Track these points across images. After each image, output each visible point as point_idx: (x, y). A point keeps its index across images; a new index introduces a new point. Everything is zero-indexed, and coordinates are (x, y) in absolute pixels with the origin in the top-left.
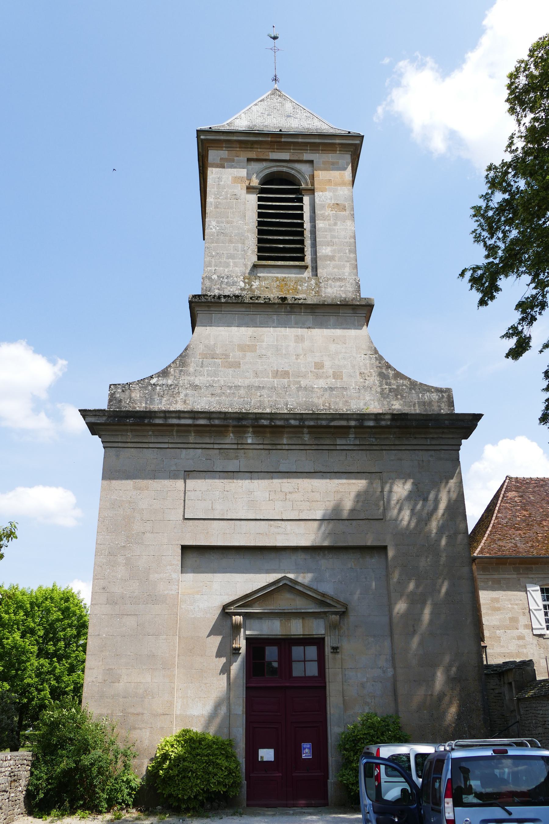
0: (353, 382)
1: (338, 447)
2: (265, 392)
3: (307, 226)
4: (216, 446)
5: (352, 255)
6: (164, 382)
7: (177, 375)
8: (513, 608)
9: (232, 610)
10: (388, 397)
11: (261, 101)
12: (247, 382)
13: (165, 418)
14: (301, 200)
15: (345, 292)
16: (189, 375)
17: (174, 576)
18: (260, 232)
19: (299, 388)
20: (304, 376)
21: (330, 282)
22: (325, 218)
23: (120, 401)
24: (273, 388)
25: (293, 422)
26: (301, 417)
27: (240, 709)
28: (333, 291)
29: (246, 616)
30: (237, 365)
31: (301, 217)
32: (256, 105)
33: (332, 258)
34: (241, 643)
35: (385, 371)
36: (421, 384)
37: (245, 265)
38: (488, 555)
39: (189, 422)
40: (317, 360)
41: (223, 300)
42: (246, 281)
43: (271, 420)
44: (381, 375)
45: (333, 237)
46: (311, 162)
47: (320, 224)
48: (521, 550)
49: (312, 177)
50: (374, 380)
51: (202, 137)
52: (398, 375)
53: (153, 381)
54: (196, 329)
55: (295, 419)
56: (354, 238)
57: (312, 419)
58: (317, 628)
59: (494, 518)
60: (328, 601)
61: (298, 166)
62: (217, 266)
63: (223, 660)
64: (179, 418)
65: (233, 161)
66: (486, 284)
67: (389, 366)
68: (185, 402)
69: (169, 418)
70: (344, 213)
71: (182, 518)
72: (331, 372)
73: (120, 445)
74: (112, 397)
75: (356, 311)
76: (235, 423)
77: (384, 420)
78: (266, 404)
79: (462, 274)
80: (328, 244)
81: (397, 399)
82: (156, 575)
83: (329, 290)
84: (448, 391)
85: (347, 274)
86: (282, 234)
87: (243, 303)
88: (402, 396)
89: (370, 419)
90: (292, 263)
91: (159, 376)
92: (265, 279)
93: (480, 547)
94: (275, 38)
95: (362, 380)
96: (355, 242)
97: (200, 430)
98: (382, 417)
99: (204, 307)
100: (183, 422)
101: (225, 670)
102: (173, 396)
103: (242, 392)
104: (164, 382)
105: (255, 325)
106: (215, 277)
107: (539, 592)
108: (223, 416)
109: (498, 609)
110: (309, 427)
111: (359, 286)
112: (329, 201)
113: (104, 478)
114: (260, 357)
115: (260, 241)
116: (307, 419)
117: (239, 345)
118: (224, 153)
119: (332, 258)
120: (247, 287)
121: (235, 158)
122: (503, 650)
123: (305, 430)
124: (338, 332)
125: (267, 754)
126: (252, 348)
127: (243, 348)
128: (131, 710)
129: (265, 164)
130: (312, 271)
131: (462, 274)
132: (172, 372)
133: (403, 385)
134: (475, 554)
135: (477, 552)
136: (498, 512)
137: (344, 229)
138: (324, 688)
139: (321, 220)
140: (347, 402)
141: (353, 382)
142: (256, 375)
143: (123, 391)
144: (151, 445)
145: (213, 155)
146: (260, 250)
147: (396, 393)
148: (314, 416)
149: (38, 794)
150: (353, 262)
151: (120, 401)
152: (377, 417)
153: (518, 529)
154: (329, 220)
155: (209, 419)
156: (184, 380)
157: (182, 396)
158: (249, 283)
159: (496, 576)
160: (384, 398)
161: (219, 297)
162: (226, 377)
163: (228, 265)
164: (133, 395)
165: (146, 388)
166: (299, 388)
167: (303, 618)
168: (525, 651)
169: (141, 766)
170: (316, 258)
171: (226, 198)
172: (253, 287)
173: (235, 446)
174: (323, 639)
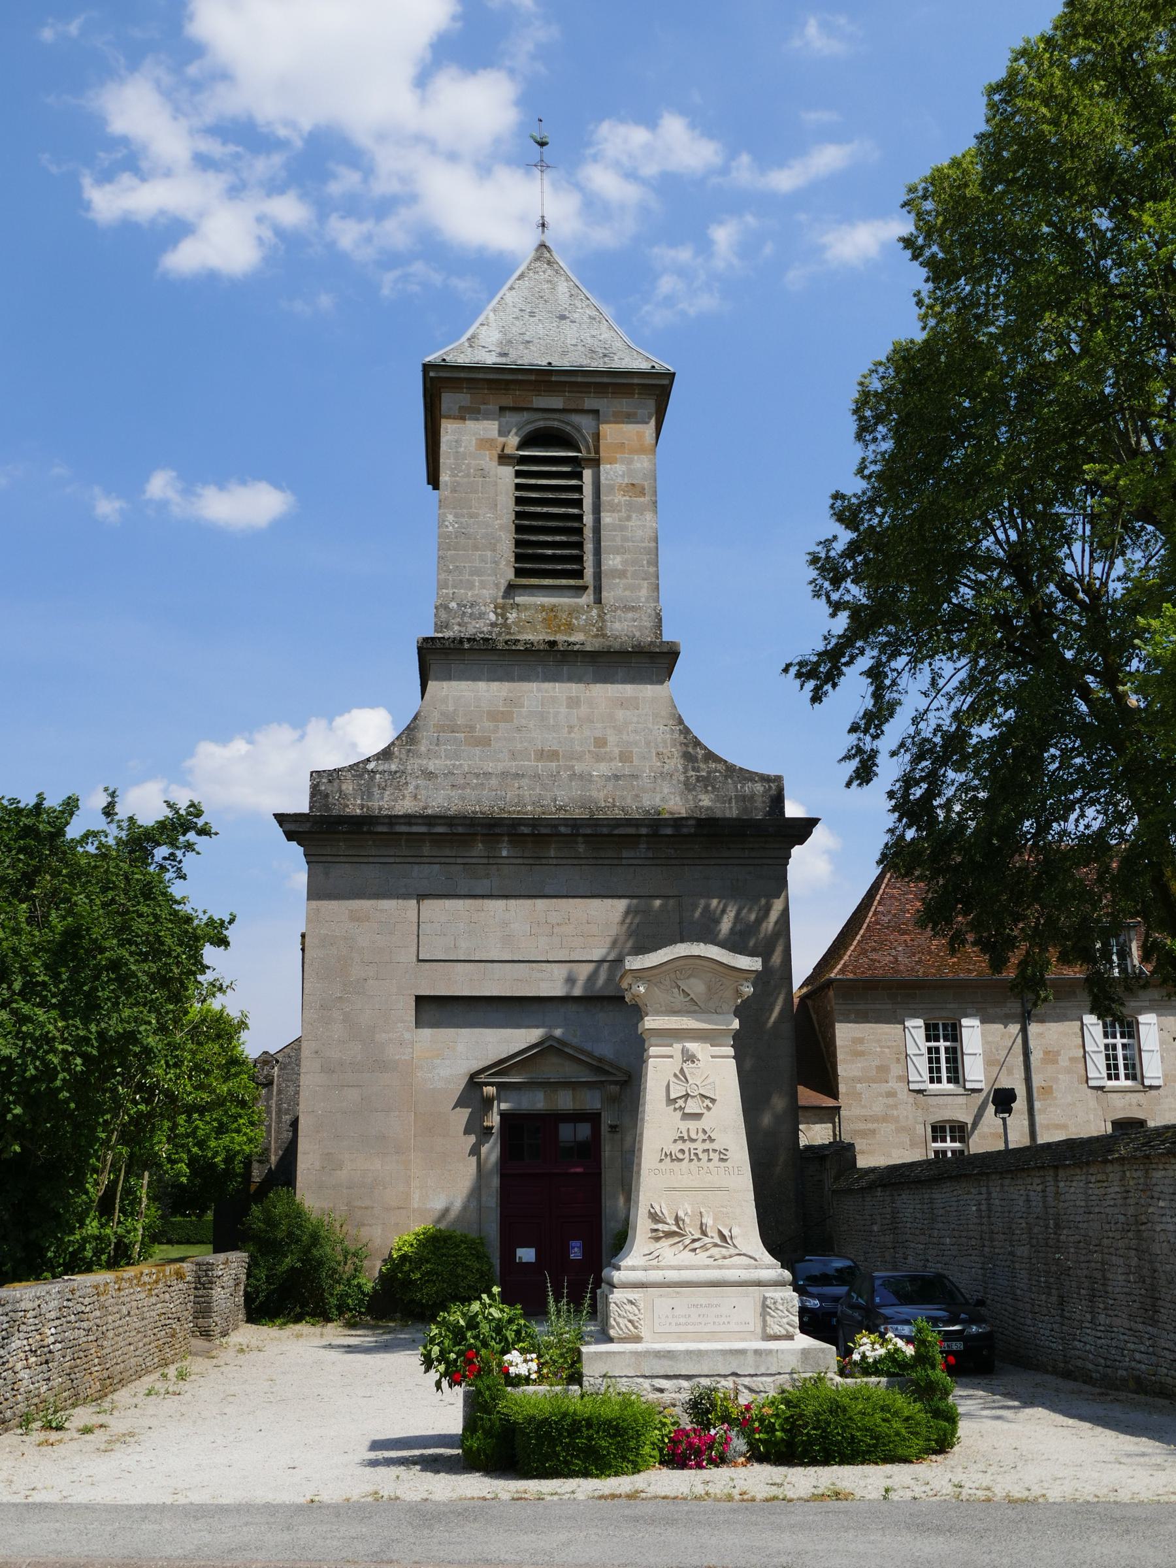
0: (647, 767)
1: (624, 862)
2: (525, 782)
3: (588, 519)
4: (459, 861)
5: (652, 569)
6: (386, 767)
7: (403, 756)
8: (883, 1052)
9: (482, 1078)
10: (694, 789)
11: (518, 279)
12: (500, 767)
13: (391, 824)
14: (579, 476)
15: (640, 628)
16: (420, 756)
17: (407, 1036)
18: (519, 529)
19: (573, 776)
20: (580, 759)
21: (619, 612)
22: (614, 508)
23: (327, 796)
24: (537, 776)
25: (563, 830)
26: (574, 823)
27: (492, 1200)
28: (624, 628)
29: (500, 1086)
30: (485, 742)
31: (579, 503)
32: (511, 288)
33: (622, 574)
34: (494, 1120)
35: (693, 750)
36: (741, 769)
37: (497, 585)
38: (851, 976)
39: (423, 829)
40: (598, 734)
41: (466, 646)
42: (499, 611)
43: (534, 826)
44: (688, 757)
45: (625, 539)
46: (596, 412)
47: (607, 518)
48: (902, 968)
49: (597, 437)
50: (676, 763)
51: (432, 374)
52: (710, 756)
53: (371, 766)
54: (432, 685)
55: (566, 826)
56: (656, 540)
57: (588, 826)
58: (591, 1101)
59: (871, 914)
60: (607, 1068)
61: (576, 419)
62: (455, 587)
63: (472, 1139)
64: (410, 824)
65: (478, 411)
66: (820, 672)
67: (697, 743)
68: (415, 797)
69: (396, 824)
70: (642, 499)
71: (415, 959)
72: (616, 751)
73: (329, 859)
74: (315, 791)
75: (654, 660)
76: (485, 831)
77: (687, 826)
78: (527, 800)
79: (786, 670)
80: (618, 551)
81: (707, 792)
82: (384, 1035)
83: (617, 625)
84: (779, 779)
85: (643, 599)
86: (551, 542)
87: (494, 650)
88: (713, 787)
89: (666, 826)
90: (564, 582)
91: (378, 759)
92: (527, 607)
93: (842, 962)
94: (542, 144)
95: (659, 764)
96: (657, 548)
97: (438, 840)
98: (684, 822)
99: (438, 657)
100: (415, 829)
101: (475, 1151)
102: (398, 788)
103: (494, 782)
104: (386, 767)
105: (509, 678)
106: (453, 605)
107: (923, 1030)
108: (468, 822)
109: (861, 1054)
110: (585, 835)
111: (660, 620)
112: (619, 480)
113: (308, 899)
114: (518, 729)
115: (518, 543)
116: (582, 826)
117: (489, 712)
118: (463, 398)
119: (622, 574)
120: (500, 621)
121: (482, 407)
122: (864, 1112)
123: (580, 839)
124: (629, 690)
125: (526, 1255)
126: (506, 717)
127: (496, 716)
128: (359, 1203)
129: (526, 416)
130: (595, 593)
131: (786, 670)
132: (397, 753)
133: (716, 771)
134: (832, 975)
135: (836, 971)
136: (879, 903)
137: (641, 525)
138: (600, 1174)
139: (608, 511)
140: (637, 796)
141: (647, 767)
142: (513, 755)
143: (330, 781)
144: (371, 860)
145: (448, 401)
146: (519, 558)
147: (706, 782)
148: (591, 822)
149: (257, 1297)
150: (653, 580)
151: (327, 796)
152: (677, 822)
153: (905, 933)
154: (620, 511)
155: (451, 825)
156: (413, 764)
157: (411, 788)
158: (503, 616)
159: (860, 1007)
160: (690, 790)
161: (461, 641)
162: (472, 760)
163: (471, 586)
164: (344, 787)
165: (361, 776)
166: (573, 776)
167: (574, 1089)
168: (895, 1113)
169: (372, 1268)
170: (600, 573)
171: (468, 476)
172: (509, 621)
173: (485, 861)
174: (599, 1114)
